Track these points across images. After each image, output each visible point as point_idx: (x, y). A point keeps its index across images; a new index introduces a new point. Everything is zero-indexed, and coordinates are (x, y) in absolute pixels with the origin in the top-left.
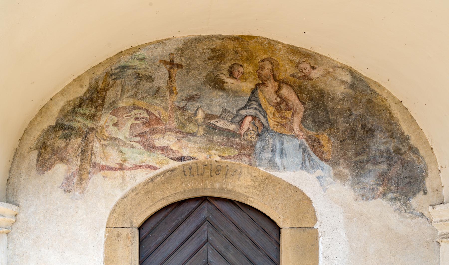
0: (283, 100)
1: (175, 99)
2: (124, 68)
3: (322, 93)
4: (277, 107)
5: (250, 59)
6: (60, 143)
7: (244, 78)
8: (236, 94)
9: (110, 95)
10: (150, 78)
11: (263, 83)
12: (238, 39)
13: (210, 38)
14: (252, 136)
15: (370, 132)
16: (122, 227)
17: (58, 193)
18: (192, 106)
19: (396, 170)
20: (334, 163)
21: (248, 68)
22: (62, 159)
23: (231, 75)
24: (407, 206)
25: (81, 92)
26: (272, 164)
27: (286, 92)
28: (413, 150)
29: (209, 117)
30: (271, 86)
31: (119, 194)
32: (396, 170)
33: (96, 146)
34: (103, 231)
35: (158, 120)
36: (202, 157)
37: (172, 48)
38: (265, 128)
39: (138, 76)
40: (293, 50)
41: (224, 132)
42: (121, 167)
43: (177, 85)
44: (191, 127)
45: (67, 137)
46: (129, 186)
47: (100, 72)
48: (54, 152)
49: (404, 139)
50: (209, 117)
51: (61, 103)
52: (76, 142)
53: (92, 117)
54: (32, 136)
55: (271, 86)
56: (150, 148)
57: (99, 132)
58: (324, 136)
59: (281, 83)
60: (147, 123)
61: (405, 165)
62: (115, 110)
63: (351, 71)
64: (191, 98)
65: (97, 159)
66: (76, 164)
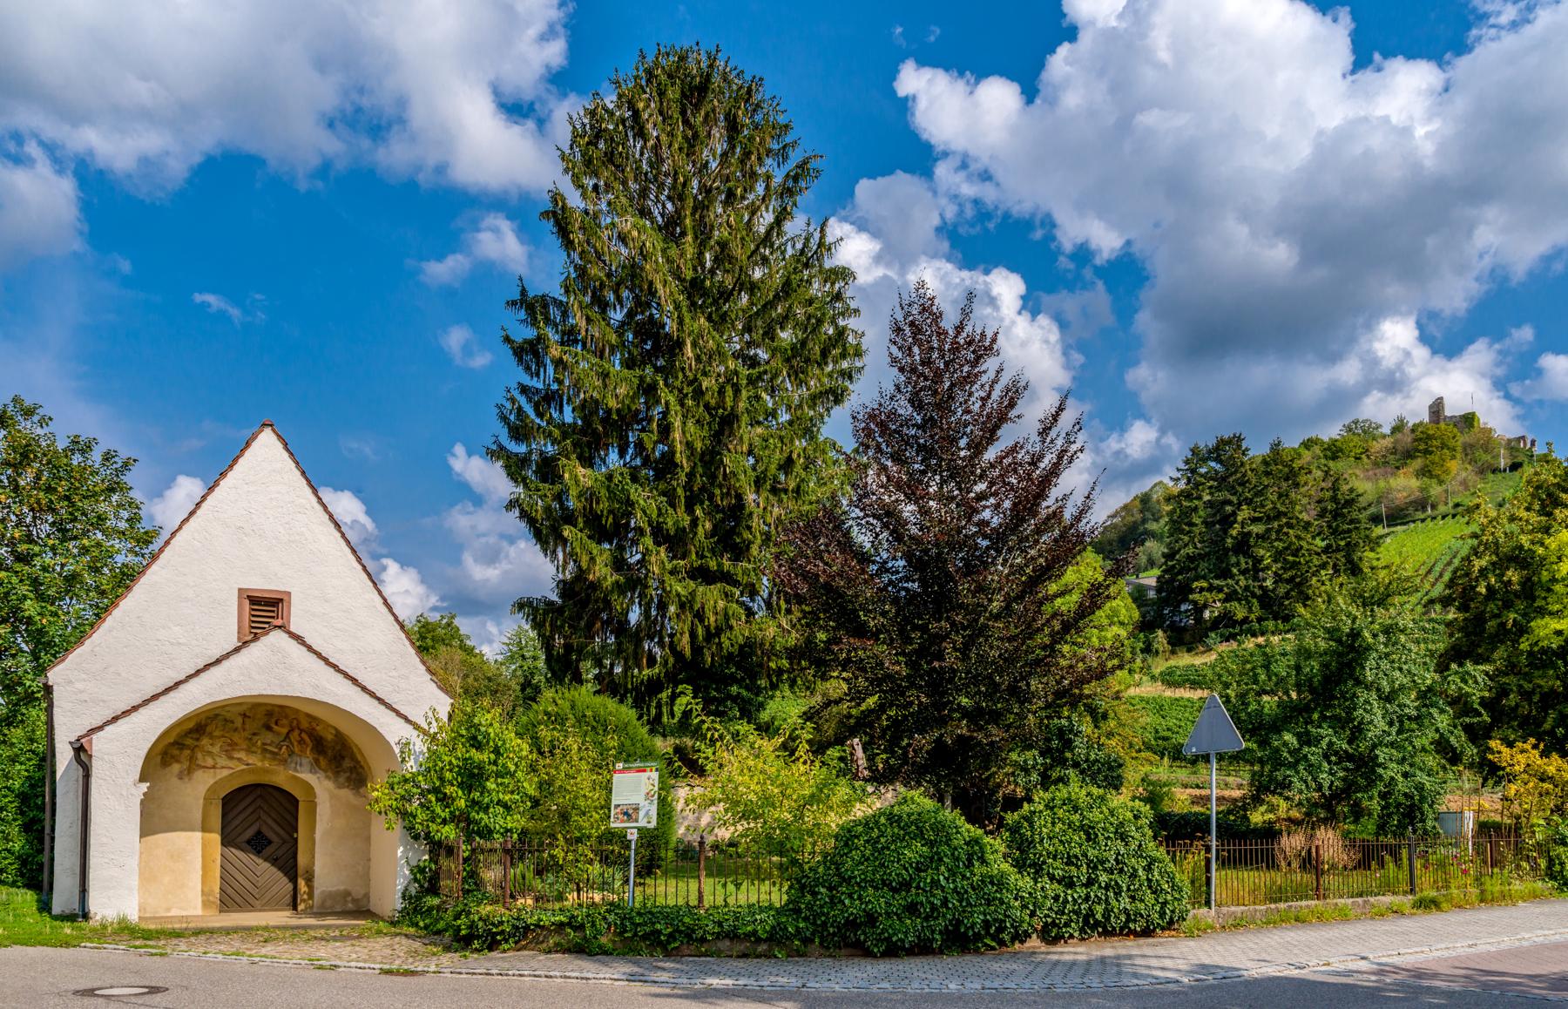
0: (302, 739)
1: (246, 734)
2: (217, 715)
3: (321, 738)
4: (299, 742)
5: (286, 717)
6: (176, 752)
7: (283, 726)
8: (279, 734)
9: (208, 729)
10: (232, 722)
11: (292, 730)
12: (281, 707)
13: (266, 704)
14: (286, 755)
15: (343, 758)
16: (225, 664)
17: (175, 781)
18: (256, 738)
19: (354, 776)
20: (325, 771)
21: (285, 722)
22: (178, 761)
23: (276, 724)
24: (358, 792)
25: (191, 725)
26: (296, 770)
27: (304, 736)
28: (361, 767)
29: (264, 744)
30: (296, 733)
31: (212, 781)
32: (354, 776)
33: (199, 755)
34: (202, 801)
35: (236, 744)
36: (259, 764)
37: (245, 707)
38: (293, 752)
39: (226, 720)
40: (308, 715)
41: (273, 753)
42: (214, 767)
43: (247, 726)
44: (254, 749)
45: (182, 749)
46: (219, 777)
47: (203, 716)
48: (173, 757)
49: (358, 762)
50: (264, 744)
51: (178, 730)
52: (187, 752)
53: (198, 739)
54: (808, 742)
55: (296, 733)
56: (231, 758)
57: (1498, 621)
58: (321, 759)
59: (301, 731)
60: (229, 745)
61: (358, 774)
62: (211, 736)
63: (336, 729)
64: (254, 734)
65: (200, 762)
66: (186, 765)
